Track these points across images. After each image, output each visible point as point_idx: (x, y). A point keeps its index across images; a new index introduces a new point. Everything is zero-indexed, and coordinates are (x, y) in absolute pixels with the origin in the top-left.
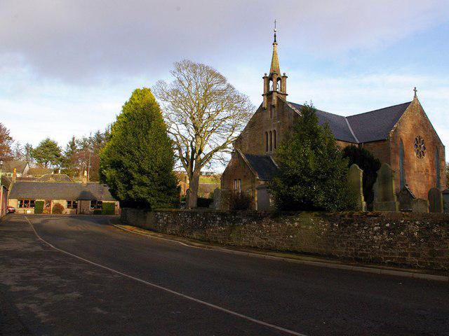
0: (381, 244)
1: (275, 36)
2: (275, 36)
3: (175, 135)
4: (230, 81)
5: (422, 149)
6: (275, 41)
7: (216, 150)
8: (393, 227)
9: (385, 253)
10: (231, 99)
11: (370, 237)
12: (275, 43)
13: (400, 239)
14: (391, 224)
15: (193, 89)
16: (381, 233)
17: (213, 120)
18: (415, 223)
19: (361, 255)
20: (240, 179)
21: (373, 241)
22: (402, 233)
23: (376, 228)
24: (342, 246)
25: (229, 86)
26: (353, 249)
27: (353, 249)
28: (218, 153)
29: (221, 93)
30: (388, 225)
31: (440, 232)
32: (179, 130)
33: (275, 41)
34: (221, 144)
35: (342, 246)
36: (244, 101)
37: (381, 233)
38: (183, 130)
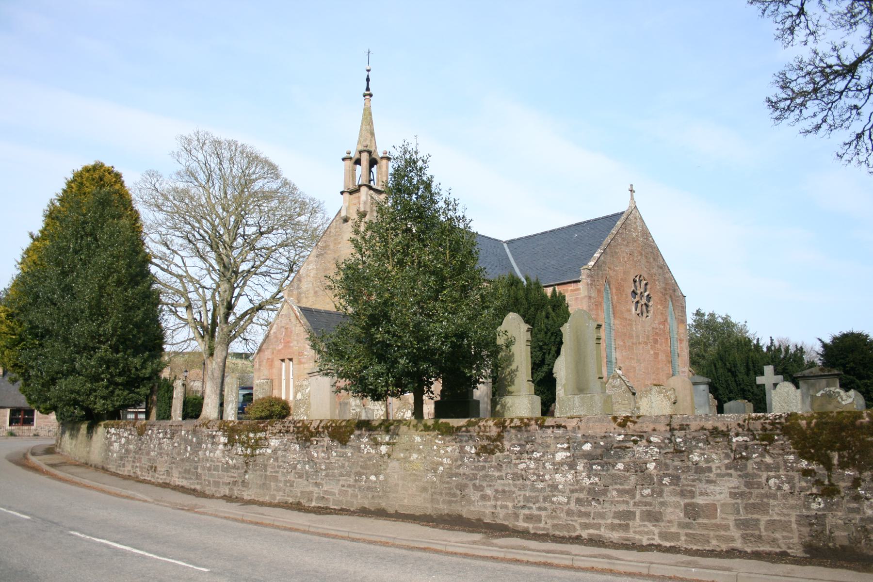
0: (572, 491)
1: (368, 80)
2: (368, 80)
3: (180, 277)
4: (286, 173)
5: (644, 301)
6: (368, 89)
7: (260, 307)
8: (599, 451)
9: (581, 514)
10: (289, 207)
11: (547, 477)
12: (368, 94)
13: (615, 479)
14: (596, 445)
15: (216, 190)
16: (572, 466)
17: (253, 248)
18: (649, 442)
19: (529, 518)
20: (291, 360)
21: (554, 487)
22: (620, 466)
23: (560, 456)
24: (484, 497)
25: (286, 183)
26: (510, 505)
27: (510, 505)
28: (263, 314)
29: (268, 196)
30: (587, 447)
31: (707, 461)
32: (179, 265)
33: (368, 89)
34: (268, 296)
35: (484, 497)
36: (314, 212)
37: (572, 466)
38: (195, 267)
